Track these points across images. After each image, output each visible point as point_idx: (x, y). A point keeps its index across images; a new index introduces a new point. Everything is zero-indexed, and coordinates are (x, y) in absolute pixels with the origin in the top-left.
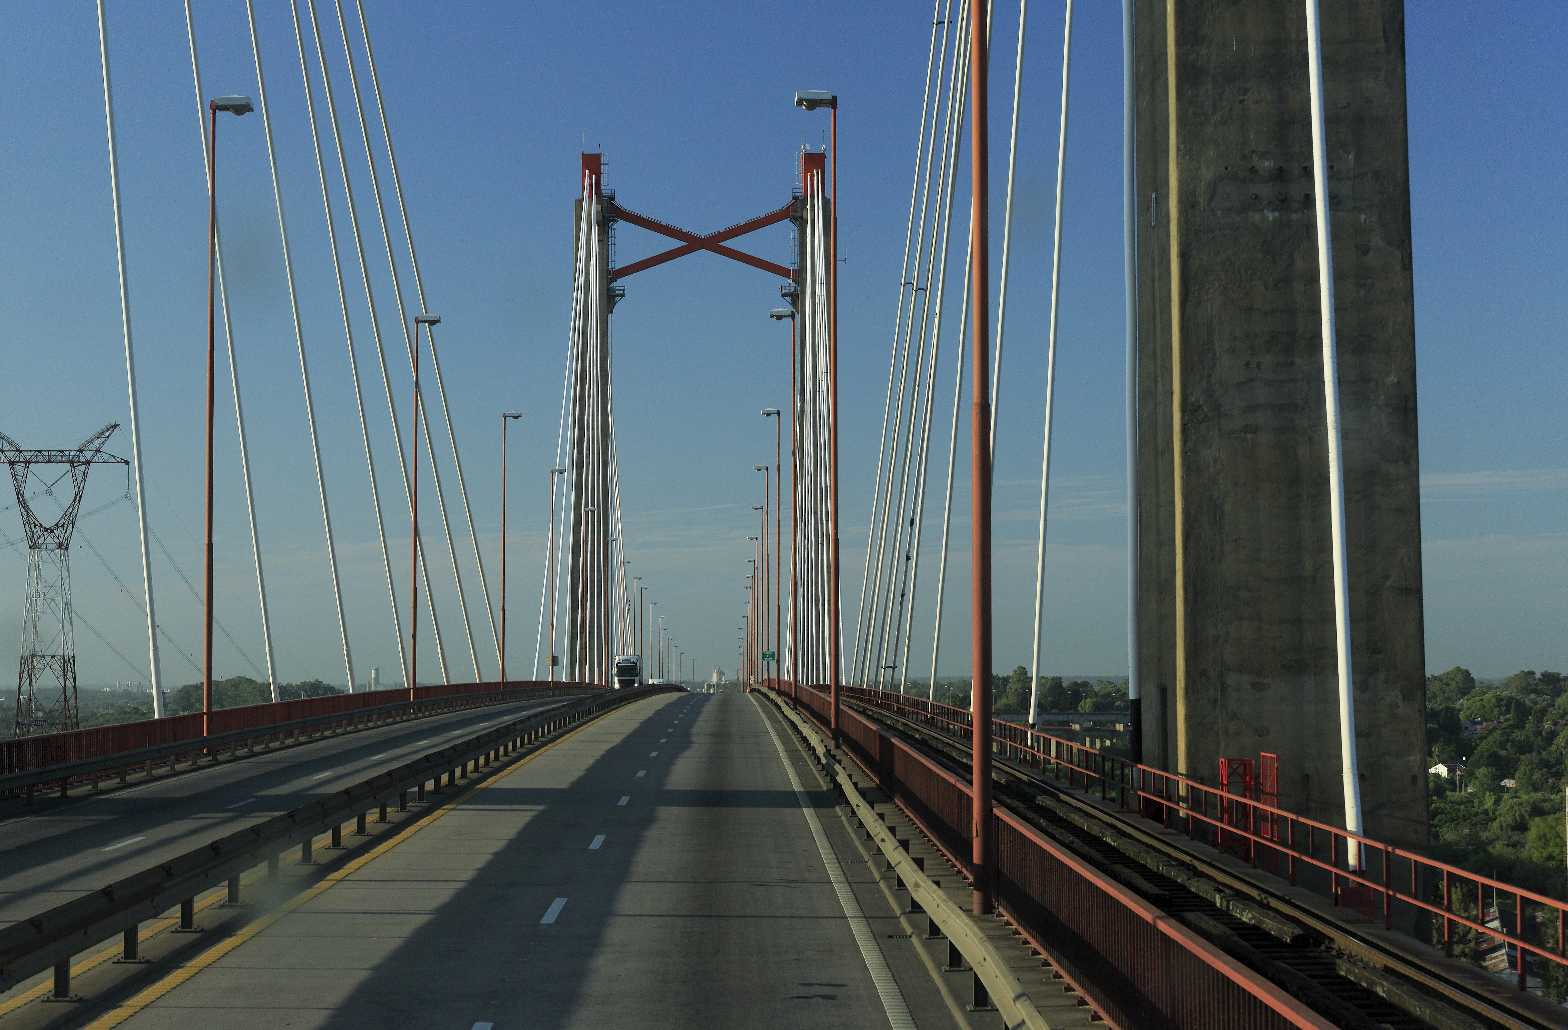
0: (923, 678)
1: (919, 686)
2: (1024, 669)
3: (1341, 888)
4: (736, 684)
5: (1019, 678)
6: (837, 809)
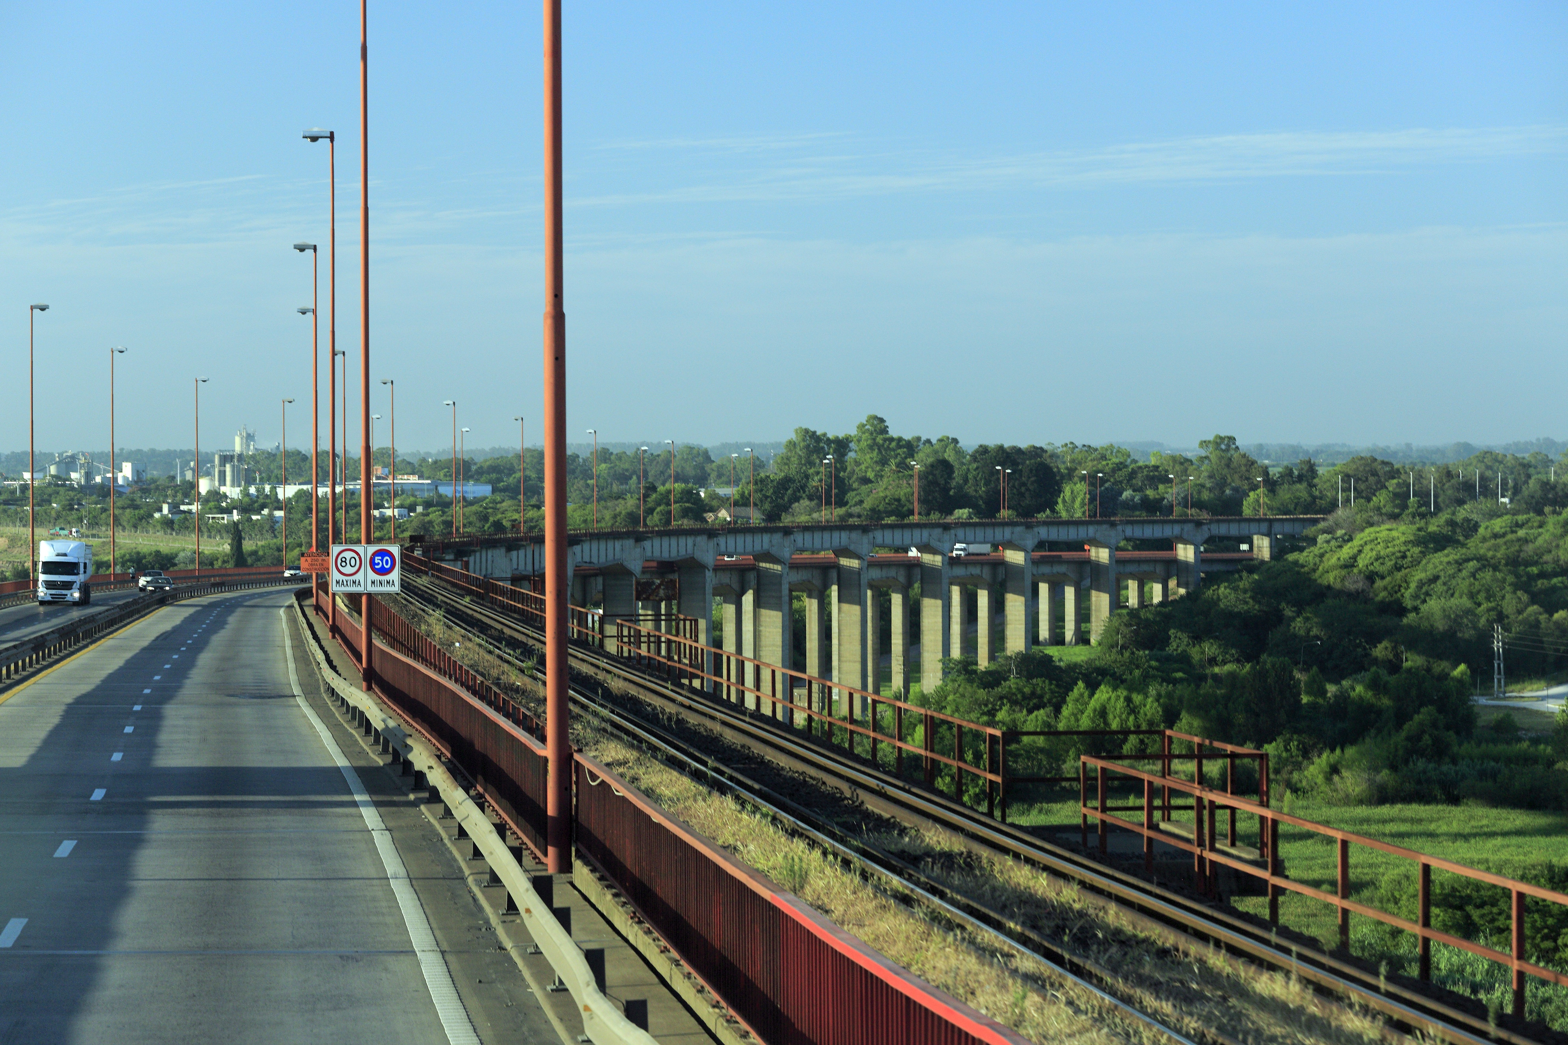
0: (444, 451)
2: (882, 420)
4: (275, 455)
5: (874, 439)
6: (381, 763)
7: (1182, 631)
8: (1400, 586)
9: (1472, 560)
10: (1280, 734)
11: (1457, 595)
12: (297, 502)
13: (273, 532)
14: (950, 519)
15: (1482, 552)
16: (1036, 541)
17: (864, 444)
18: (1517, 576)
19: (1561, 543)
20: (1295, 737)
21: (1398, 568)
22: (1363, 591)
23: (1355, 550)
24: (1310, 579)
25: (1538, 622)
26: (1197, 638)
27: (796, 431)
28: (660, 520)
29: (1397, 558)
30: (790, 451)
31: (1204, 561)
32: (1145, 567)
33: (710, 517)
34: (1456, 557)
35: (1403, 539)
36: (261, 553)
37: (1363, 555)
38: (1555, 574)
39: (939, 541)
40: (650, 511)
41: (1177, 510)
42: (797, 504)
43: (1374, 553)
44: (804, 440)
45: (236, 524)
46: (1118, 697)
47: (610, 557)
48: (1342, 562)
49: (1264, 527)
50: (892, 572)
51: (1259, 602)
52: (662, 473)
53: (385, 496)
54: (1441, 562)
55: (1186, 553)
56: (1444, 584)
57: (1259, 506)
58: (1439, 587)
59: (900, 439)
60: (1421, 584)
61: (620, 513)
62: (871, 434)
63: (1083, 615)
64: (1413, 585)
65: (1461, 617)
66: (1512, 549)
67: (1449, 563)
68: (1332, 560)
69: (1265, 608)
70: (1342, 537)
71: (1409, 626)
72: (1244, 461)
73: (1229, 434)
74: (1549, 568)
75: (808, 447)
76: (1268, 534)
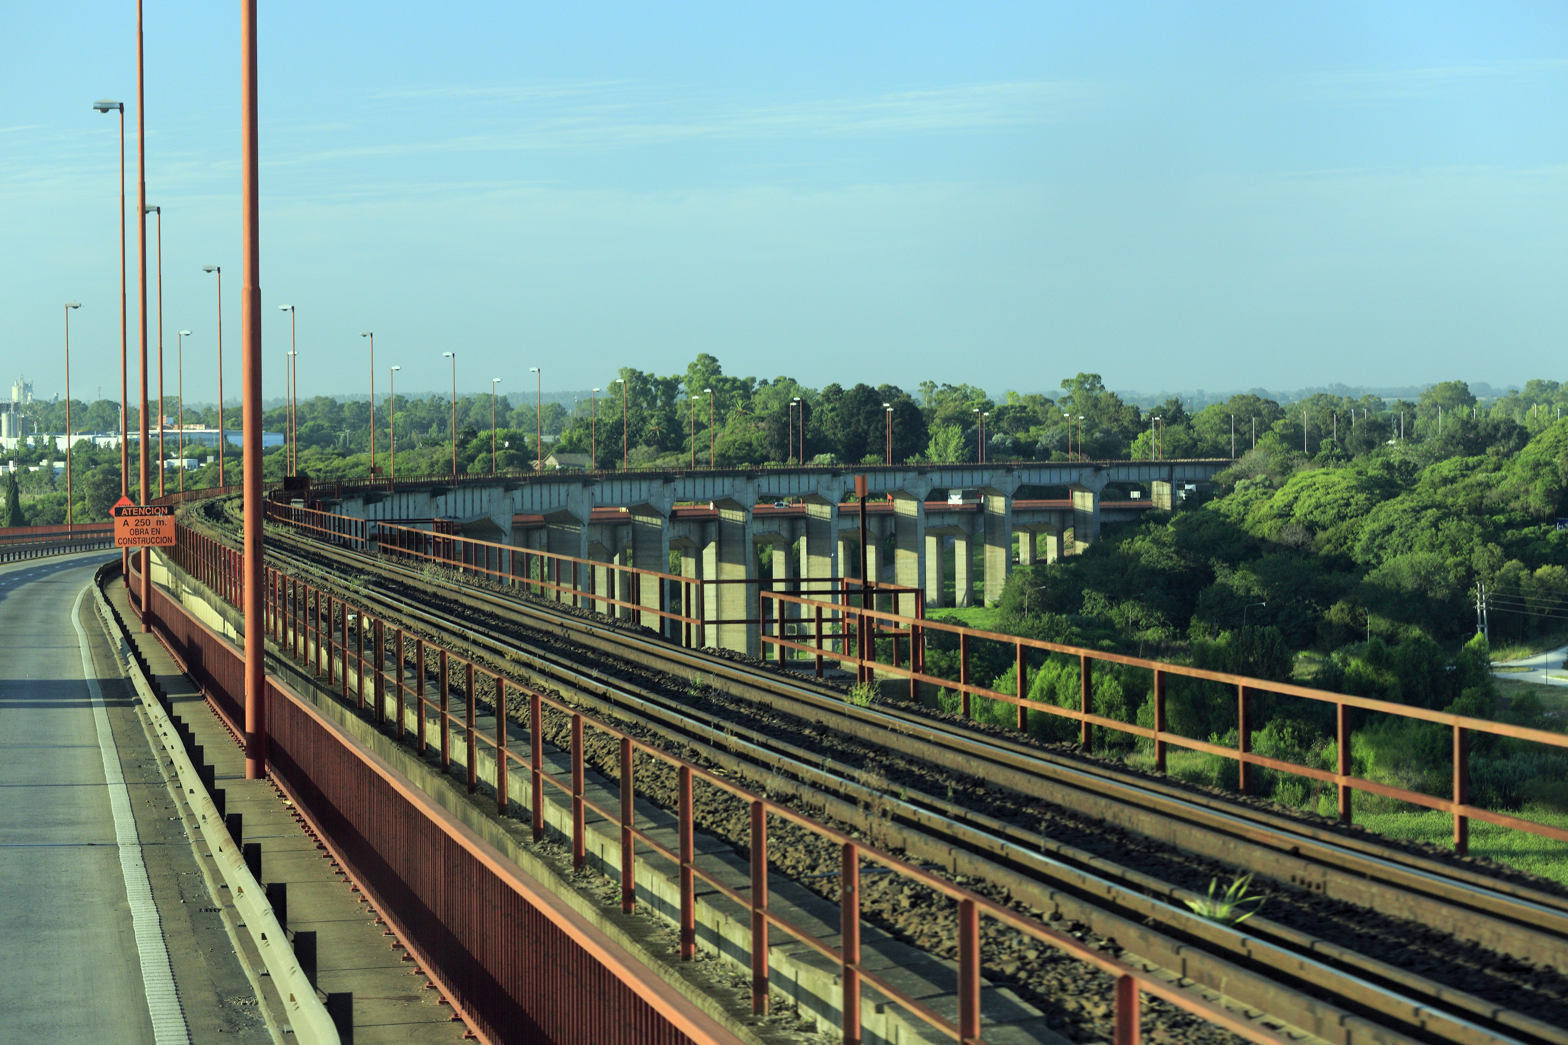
1: (408, 405)
2: (714, 360)
3: (887, 939)
5: (707, 380)
7: (1098, 591)
8: (1346, 538)
9: (1431, 507)
10: (1270, 719)
11: (1416, 548)
12: (78, 452)
13: (53, 484)
14: (810, 465)
15: (1438, 498)
16: (929, 489)
17: (695, 385)
18: (1483, 525)
19: (1531, 487)
20: (1288, 722)
21: (1342, 518)
22: (1303, 543)
23: (1291, 497)
24: (1239, 531)
25: (1518, 578)
26: (1114, 599)
27: (621, 371)
28: (482, 468)
29: (1340, 506)
30: (615, 393)
31: (1103, 510)
32: (1039, 518)
33: (536, 464)
34: (1414, 504)
35: (1344, 484)
36: (39, 507)
37: (1300, 503)
38: (1526, 524)
39: (828, 489)
40: (471, 459)
41: (1055, 454)
42: (634, 450)
43: (1313, 500)
44: (630, 381)
45: (12, 476)
46: (1070, 676)
47: (477, 510)
48: (1275, 512)
49: (1165, 472)
50: (774, 526)
51: (1184, 557)
52: (461, 421)
53: (172, 446)
54: (1396, 511)
55: (1084, 501)
56: (1401, 535)
57: (1150, 449)
58: (1394, 539)
59: (735, 380)
60: (1373, 537)
61: (438, 461)
62: (703, 374)
63: (976, 572)
64: (1364, 537)
65: (1433, 574)
66: (1474, 495)
67: (1404, 511)
68: (1264, 508)
69: (1192, 565)
70: (1263, 482)
71: (1372, 585)
72: (1112, 401)
73: (1094, 373)
74: (1518, 516)
75: (633, 389)
76: (1169, 480)
